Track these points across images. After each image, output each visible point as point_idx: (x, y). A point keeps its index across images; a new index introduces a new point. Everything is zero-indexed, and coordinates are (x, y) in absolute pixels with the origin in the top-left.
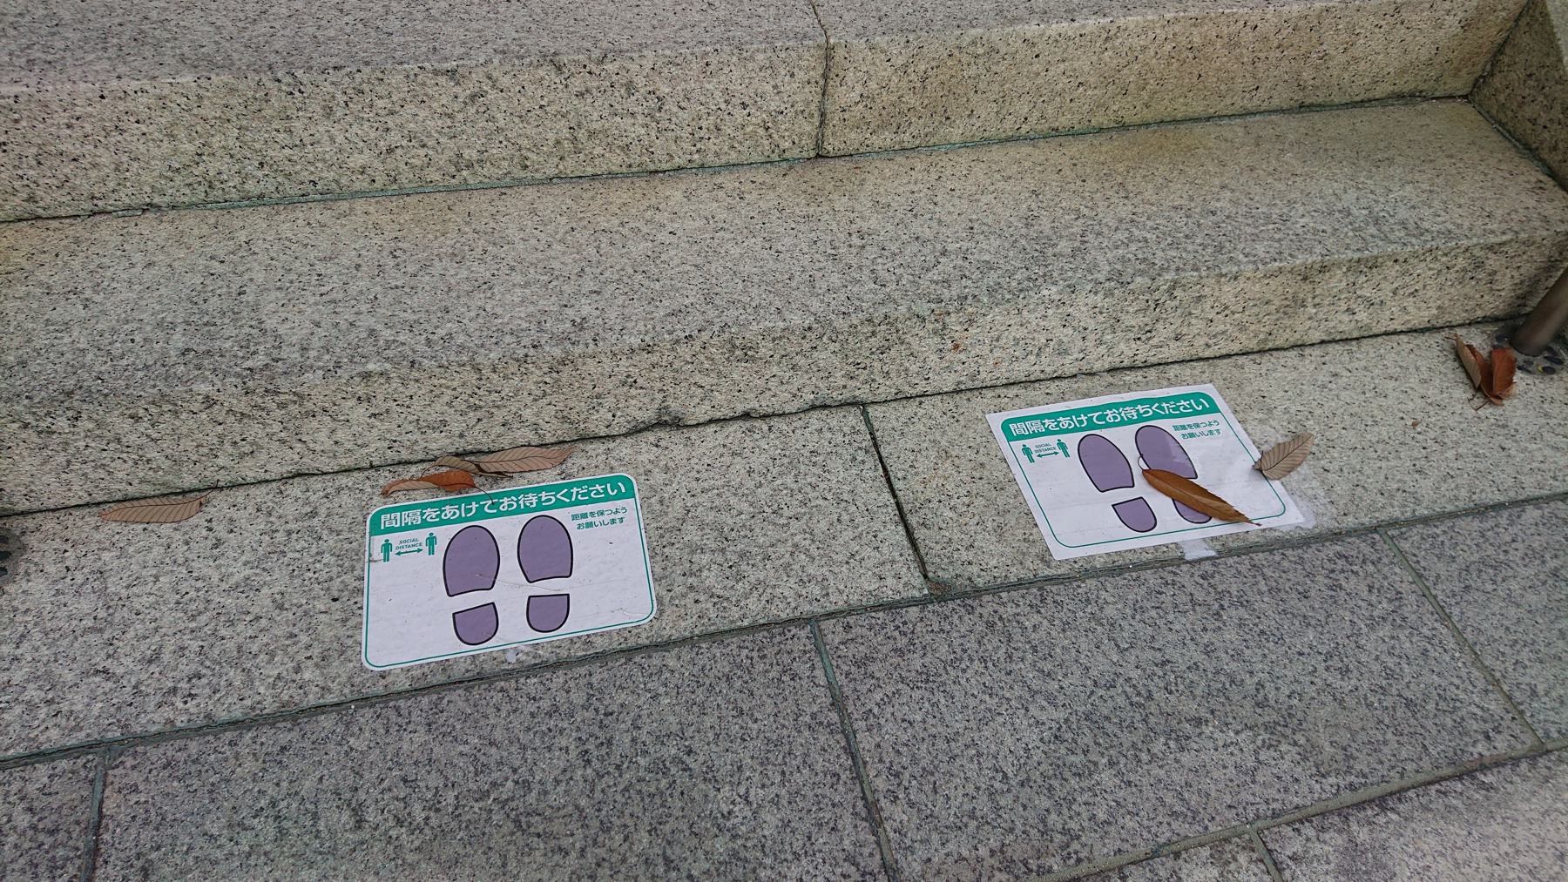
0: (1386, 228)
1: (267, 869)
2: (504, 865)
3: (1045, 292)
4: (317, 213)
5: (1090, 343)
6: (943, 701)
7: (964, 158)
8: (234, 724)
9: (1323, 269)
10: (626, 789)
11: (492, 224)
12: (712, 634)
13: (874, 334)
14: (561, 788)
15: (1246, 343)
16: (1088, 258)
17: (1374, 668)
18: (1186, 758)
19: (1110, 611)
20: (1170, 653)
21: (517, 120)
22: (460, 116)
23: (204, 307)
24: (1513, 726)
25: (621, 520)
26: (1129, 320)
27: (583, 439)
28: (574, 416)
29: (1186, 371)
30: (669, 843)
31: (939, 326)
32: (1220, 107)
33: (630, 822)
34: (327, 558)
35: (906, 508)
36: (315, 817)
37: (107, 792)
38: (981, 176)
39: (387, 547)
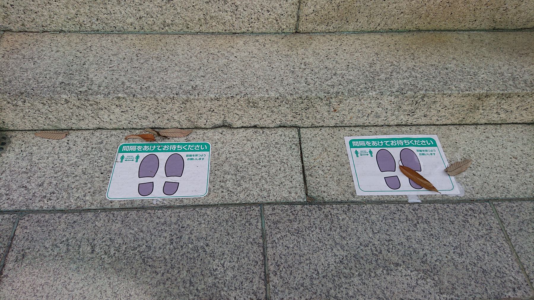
0: (517, 82)
1: (61, 262)
2: (136, 274)
3: (371, 94)
4: (116, 38)
5: (389, 114)
6: (302, 241)
7: (353, 37)
8: (62, 211)
9: (487, 96)
10: (183, 255)
11: (173, 48)
12: (225, 204)
13: (302, 103)
14: (161, 251)
15: (454, 121)
16: (391, 82)
17: (473, 255)
18: (389, 278)
19: (373, 217)
20: (393, 237)
21: (184, 10)
22: (164, 7)
23: (71, 68)
24: (526, 288)
25: (203, 159)
26: (405, 107)
27: (196, 128)
28: (192, 120)
29: (428, 129)
30: (193, 276)
31: (328, 102)
32: (459, 26)
33: (181, 267)
34: (103, 159)
35: (306, 168)
36: (80, 247)
37: (18, 228)
38: (357, 45)
39: (122, 158)
